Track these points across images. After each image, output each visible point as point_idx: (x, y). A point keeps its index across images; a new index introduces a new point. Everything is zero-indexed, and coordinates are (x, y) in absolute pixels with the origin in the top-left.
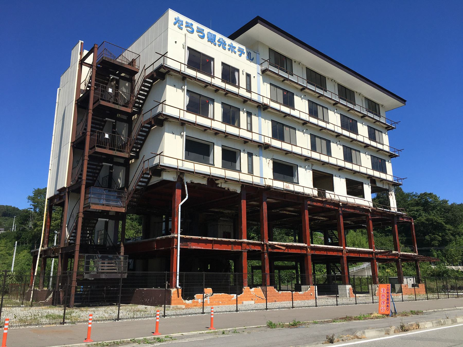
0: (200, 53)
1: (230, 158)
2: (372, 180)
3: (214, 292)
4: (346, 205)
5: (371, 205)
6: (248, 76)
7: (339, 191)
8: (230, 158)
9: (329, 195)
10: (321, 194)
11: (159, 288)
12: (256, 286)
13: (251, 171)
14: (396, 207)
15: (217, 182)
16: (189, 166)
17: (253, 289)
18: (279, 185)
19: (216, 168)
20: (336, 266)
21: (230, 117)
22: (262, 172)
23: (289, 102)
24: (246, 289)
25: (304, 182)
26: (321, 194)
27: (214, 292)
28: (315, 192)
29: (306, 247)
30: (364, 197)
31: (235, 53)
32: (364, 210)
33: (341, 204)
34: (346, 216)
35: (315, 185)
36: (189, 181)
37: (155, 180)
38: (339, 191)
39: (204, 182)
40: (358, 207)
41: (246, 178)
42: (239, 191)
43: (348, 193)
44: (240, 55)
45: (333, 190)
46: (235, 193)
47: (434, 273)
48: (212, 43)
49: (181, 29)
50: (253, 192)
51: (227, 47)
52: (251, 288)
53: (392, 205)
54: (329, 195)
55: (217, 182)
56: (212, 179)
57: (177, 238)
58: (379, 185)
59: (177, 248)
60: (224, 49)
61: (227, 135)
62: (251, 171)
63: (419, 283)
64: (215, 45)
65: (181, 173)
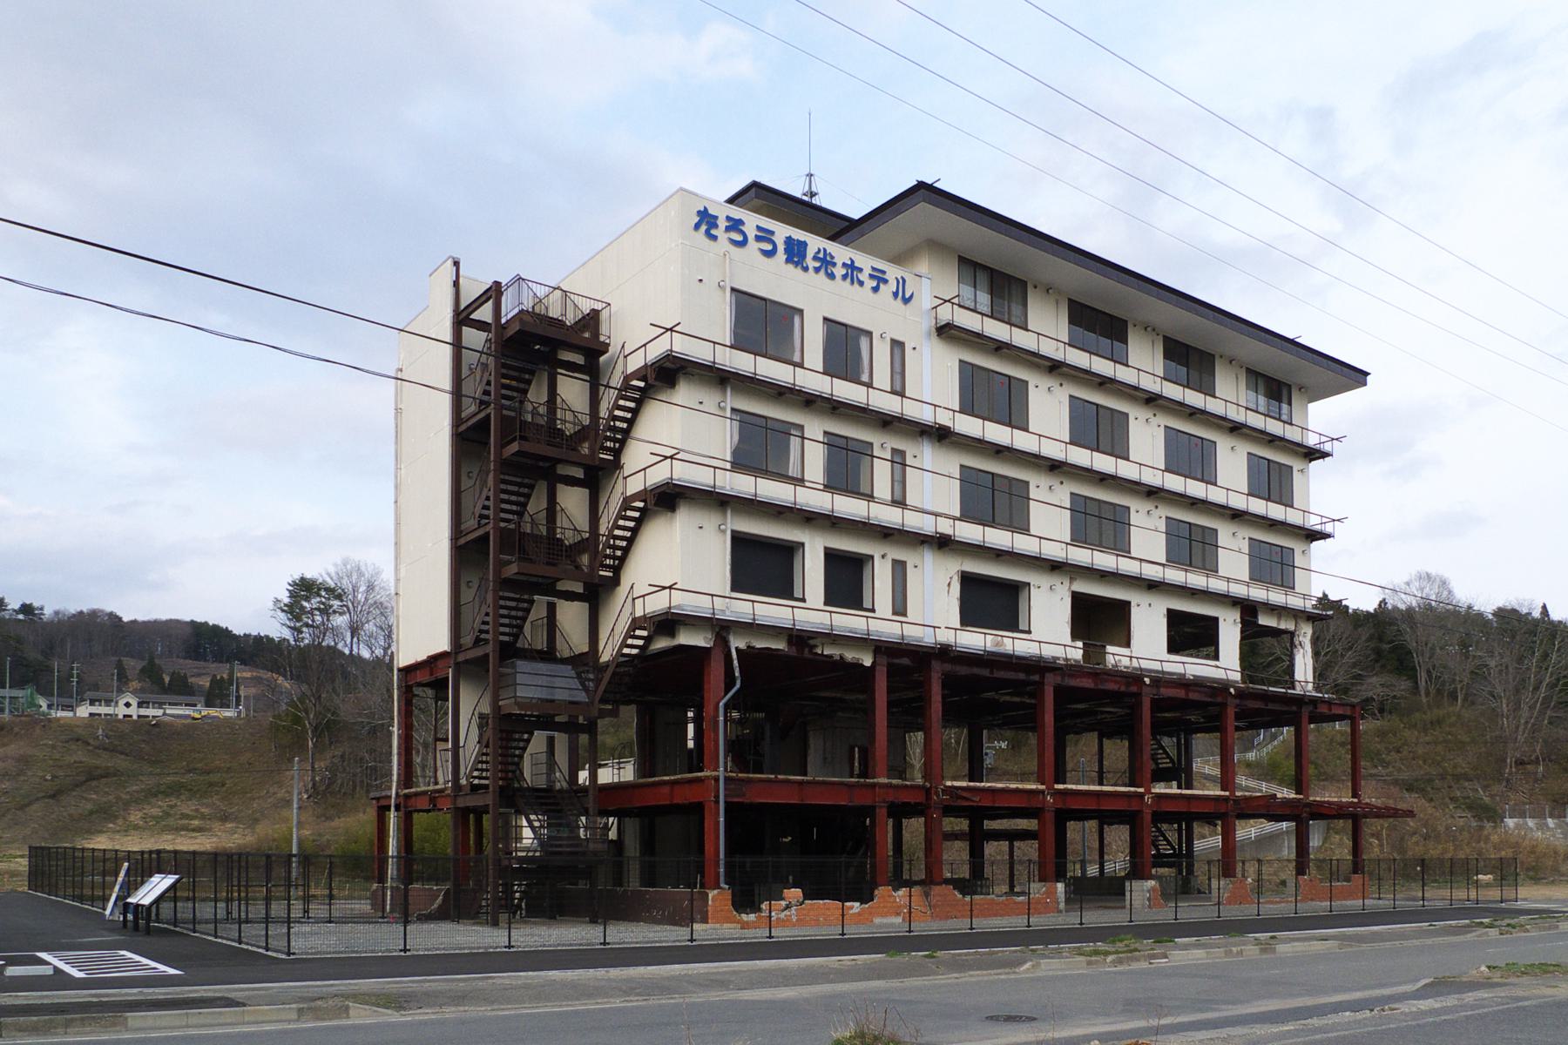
0: (845, 325)
1: (846, 582)
2: (1248, 610)
3: (807, 896)
4: (1160, 680)
5: (1237, 677)
6: (897, 346)
7: (1147, 646)
8: (846, 582)
9: (1116, 656)
10: (1094, 651)
11: (682, 889)
12: (909, 884)
13: (900, 609)
14: (1310, 679)
15: (812, 642)
16: (744, 607)
17: (903, 892)
18: (976, 640)
19: (809, 609)
20: (1159, 830)
21: (846, 471)
22: (931, 610)
23: (1013, 412)
24: (881, 891)
25: (1047, 630)
26: (1094, 651)
27: (807, 896)
28: (1076, 653)
29: (1042, 792)
30: (1216, 658)
31: (861, 283)
32: (1220, 688)
33: (1147, 680)
34: (1159, 704)
35: (1075, 636)
36: (742, 645)
37: (661, 644)
38: (1147, 646)
39: (779, 645)
40: (1198, 683)
41: (884, 626)
42: (868, 662)
43: (736, 587)
44: (876, 289)
45: (1128, 645)
46: (858, 666)
47: (1054, 867)
48: (796, 264)
49: (714, 238)
50: (909, 663)
51: (839, 271)
52: (896, 889)
53: (1299, 676)
54: (1116, 656)
55: (812, 642)
56: (799, 638)
57: (717, 779)
58: (1264, 620)
59: (717, 802)
60: (831, 276)
61: (832, 523)
62: (900, 609)
63: (1355, 872)
64: (806, 269)
65: (722, 628)
